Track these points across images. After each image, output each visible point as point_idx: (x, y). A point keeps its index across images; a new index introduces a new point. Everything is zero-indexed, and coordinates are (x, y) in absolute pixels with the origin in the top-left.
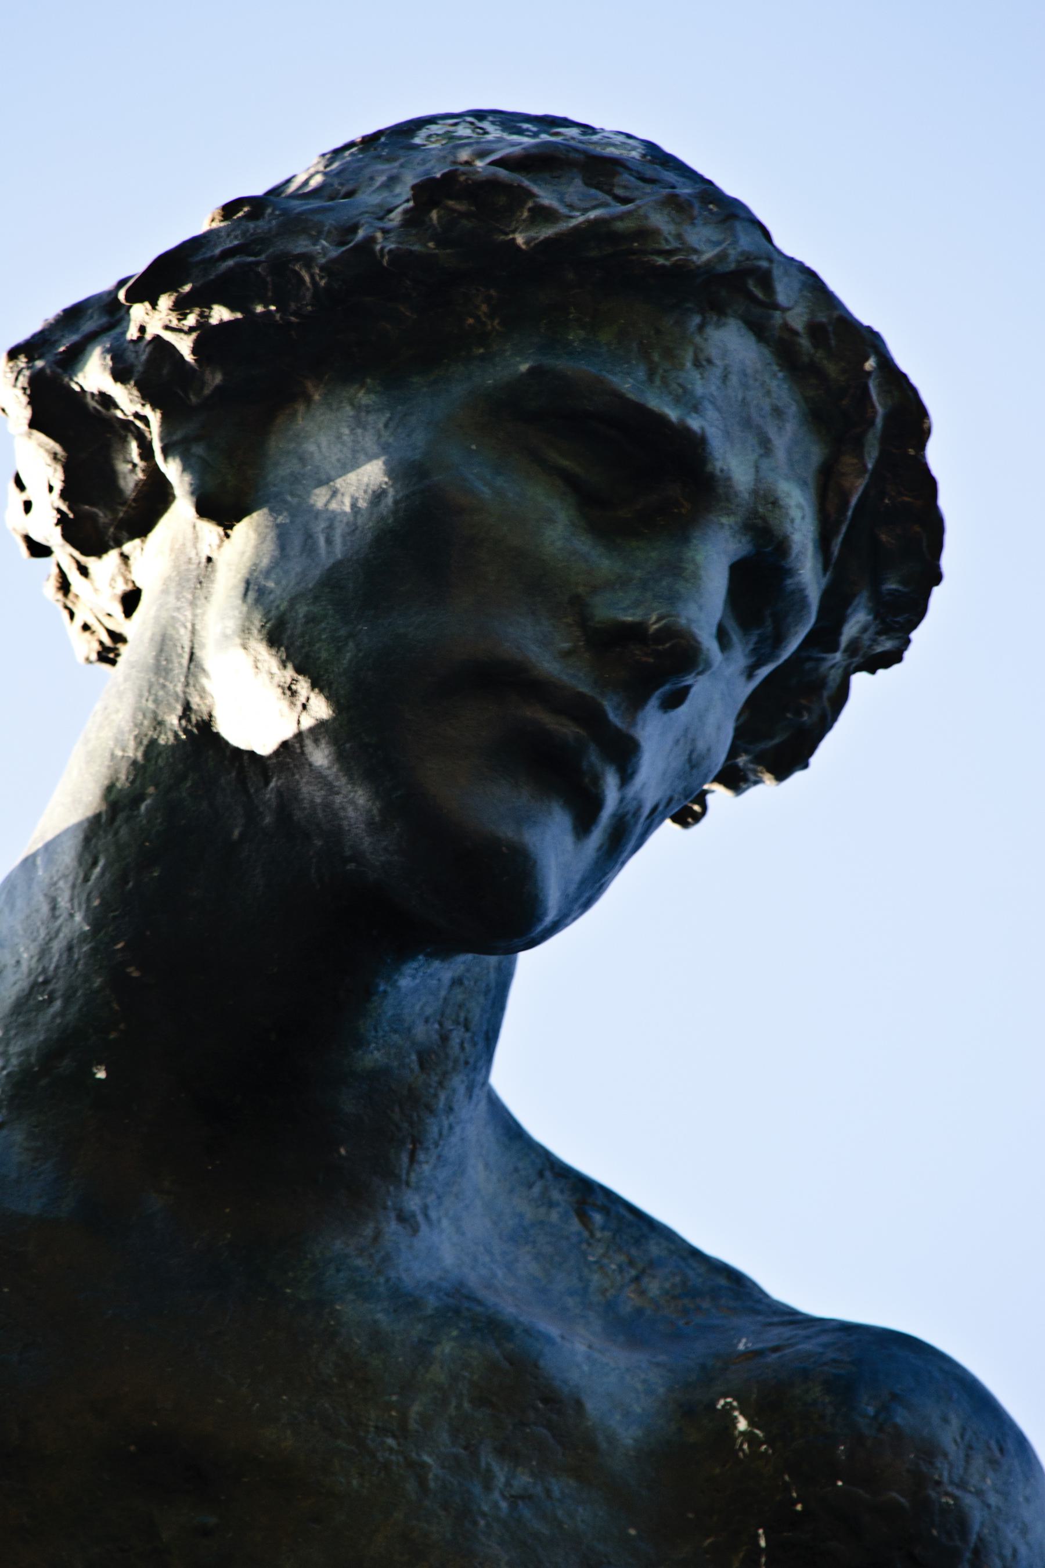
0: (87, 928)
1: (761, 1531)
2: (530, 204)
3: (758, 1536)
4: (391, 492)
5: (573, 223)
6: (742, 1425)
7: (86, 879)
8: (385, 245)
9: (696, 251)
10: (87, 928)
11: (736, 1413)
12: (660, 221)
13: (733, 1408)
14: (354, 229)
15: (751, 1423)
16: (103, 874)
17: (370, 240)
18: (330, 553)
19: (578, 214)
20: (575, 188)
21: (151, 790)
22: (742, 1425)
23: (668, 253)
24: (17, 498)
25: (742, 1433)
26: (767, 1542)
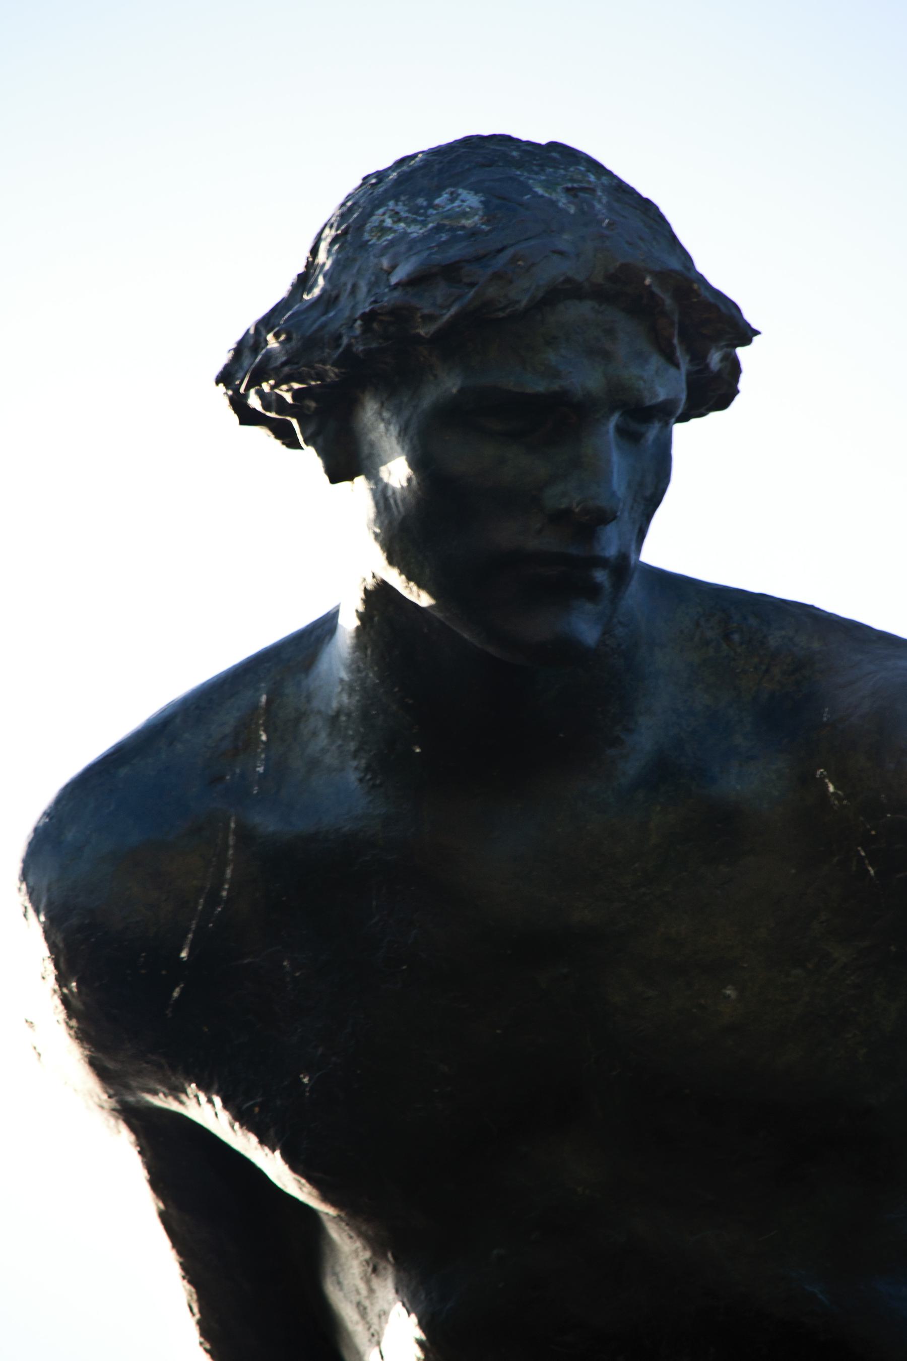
0: (377, 681)
1: (859, 848)
2: (419, 315)
3: (858, 851)
4: (414, 477)
5: (446, 318)
6: (831, 788)
7: (366, 655)
8: (359, 348)
9: (518, 302)
10: (377, 681)
11: (827, 781)
12: (492, 292)
13: (825, 777)
14: (340, 337)
15: (836, 787)
16: (372, 651)
17: (350, 346)
18: (399, 512)
19: (444, 311)
20: (441, 291)
21: (375, 613)
22: (831, 788)
23: (503, 309)
24: (38, 1050)
25: (833, 794)
26: (865, 852)
